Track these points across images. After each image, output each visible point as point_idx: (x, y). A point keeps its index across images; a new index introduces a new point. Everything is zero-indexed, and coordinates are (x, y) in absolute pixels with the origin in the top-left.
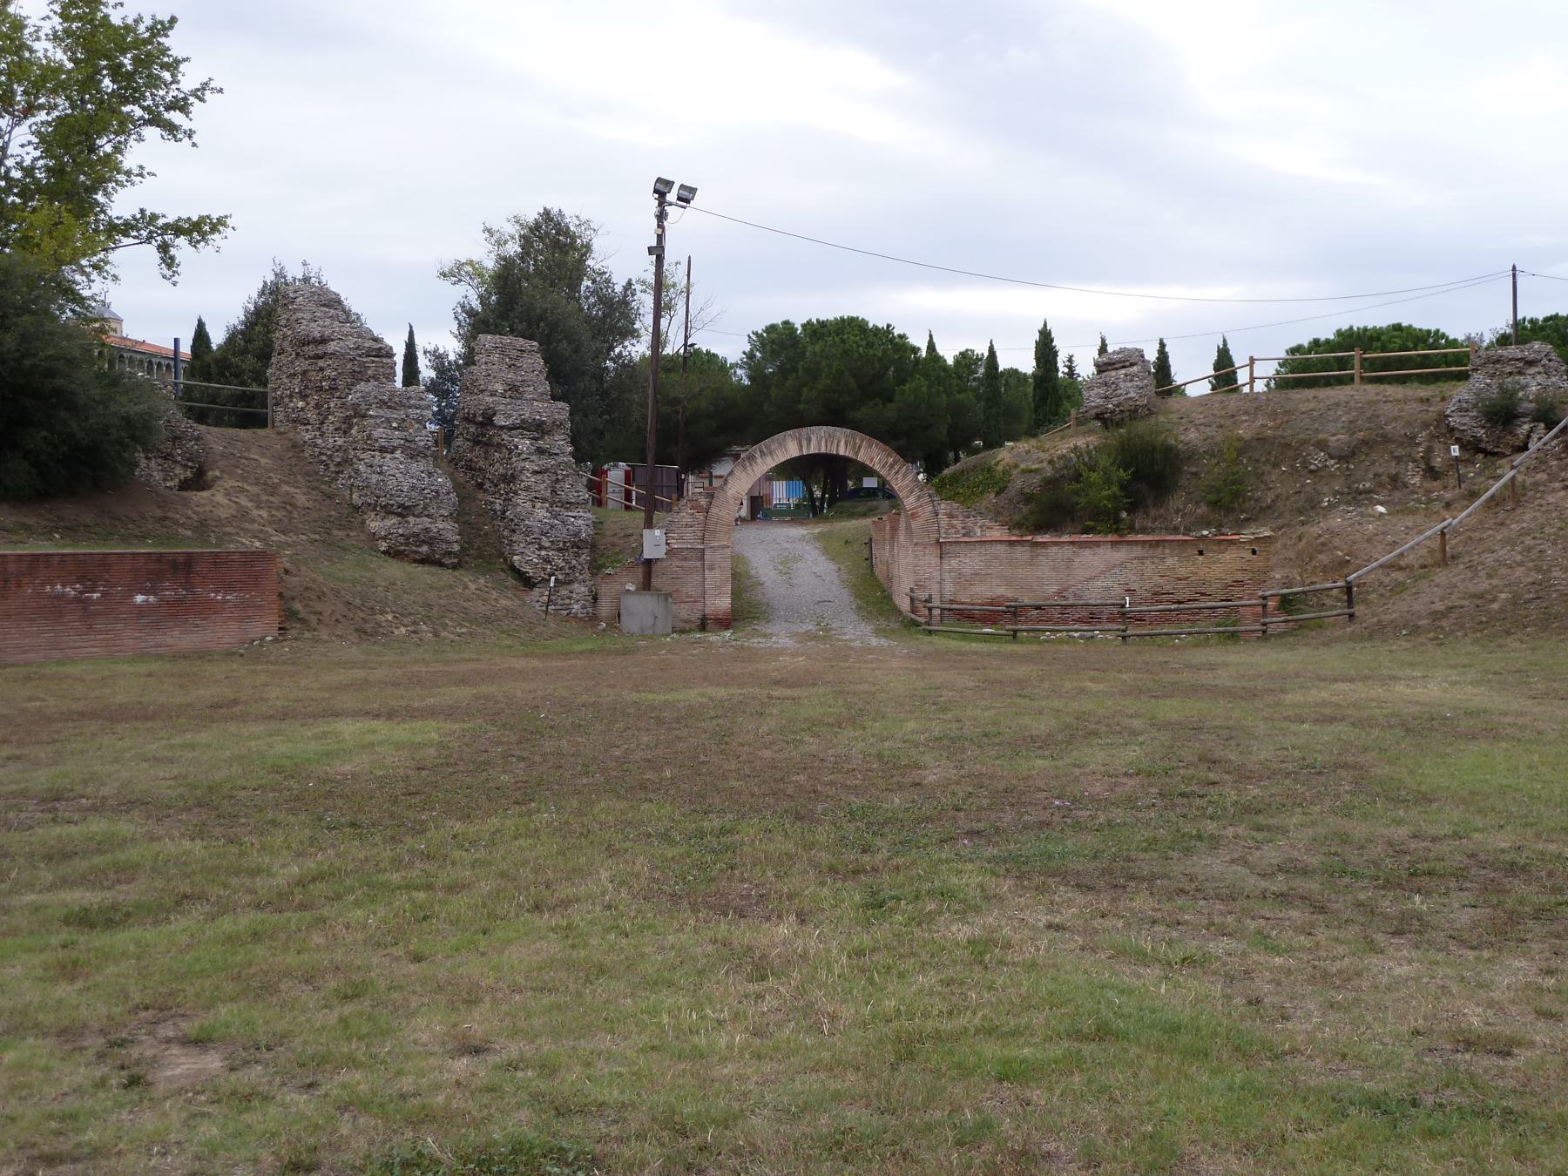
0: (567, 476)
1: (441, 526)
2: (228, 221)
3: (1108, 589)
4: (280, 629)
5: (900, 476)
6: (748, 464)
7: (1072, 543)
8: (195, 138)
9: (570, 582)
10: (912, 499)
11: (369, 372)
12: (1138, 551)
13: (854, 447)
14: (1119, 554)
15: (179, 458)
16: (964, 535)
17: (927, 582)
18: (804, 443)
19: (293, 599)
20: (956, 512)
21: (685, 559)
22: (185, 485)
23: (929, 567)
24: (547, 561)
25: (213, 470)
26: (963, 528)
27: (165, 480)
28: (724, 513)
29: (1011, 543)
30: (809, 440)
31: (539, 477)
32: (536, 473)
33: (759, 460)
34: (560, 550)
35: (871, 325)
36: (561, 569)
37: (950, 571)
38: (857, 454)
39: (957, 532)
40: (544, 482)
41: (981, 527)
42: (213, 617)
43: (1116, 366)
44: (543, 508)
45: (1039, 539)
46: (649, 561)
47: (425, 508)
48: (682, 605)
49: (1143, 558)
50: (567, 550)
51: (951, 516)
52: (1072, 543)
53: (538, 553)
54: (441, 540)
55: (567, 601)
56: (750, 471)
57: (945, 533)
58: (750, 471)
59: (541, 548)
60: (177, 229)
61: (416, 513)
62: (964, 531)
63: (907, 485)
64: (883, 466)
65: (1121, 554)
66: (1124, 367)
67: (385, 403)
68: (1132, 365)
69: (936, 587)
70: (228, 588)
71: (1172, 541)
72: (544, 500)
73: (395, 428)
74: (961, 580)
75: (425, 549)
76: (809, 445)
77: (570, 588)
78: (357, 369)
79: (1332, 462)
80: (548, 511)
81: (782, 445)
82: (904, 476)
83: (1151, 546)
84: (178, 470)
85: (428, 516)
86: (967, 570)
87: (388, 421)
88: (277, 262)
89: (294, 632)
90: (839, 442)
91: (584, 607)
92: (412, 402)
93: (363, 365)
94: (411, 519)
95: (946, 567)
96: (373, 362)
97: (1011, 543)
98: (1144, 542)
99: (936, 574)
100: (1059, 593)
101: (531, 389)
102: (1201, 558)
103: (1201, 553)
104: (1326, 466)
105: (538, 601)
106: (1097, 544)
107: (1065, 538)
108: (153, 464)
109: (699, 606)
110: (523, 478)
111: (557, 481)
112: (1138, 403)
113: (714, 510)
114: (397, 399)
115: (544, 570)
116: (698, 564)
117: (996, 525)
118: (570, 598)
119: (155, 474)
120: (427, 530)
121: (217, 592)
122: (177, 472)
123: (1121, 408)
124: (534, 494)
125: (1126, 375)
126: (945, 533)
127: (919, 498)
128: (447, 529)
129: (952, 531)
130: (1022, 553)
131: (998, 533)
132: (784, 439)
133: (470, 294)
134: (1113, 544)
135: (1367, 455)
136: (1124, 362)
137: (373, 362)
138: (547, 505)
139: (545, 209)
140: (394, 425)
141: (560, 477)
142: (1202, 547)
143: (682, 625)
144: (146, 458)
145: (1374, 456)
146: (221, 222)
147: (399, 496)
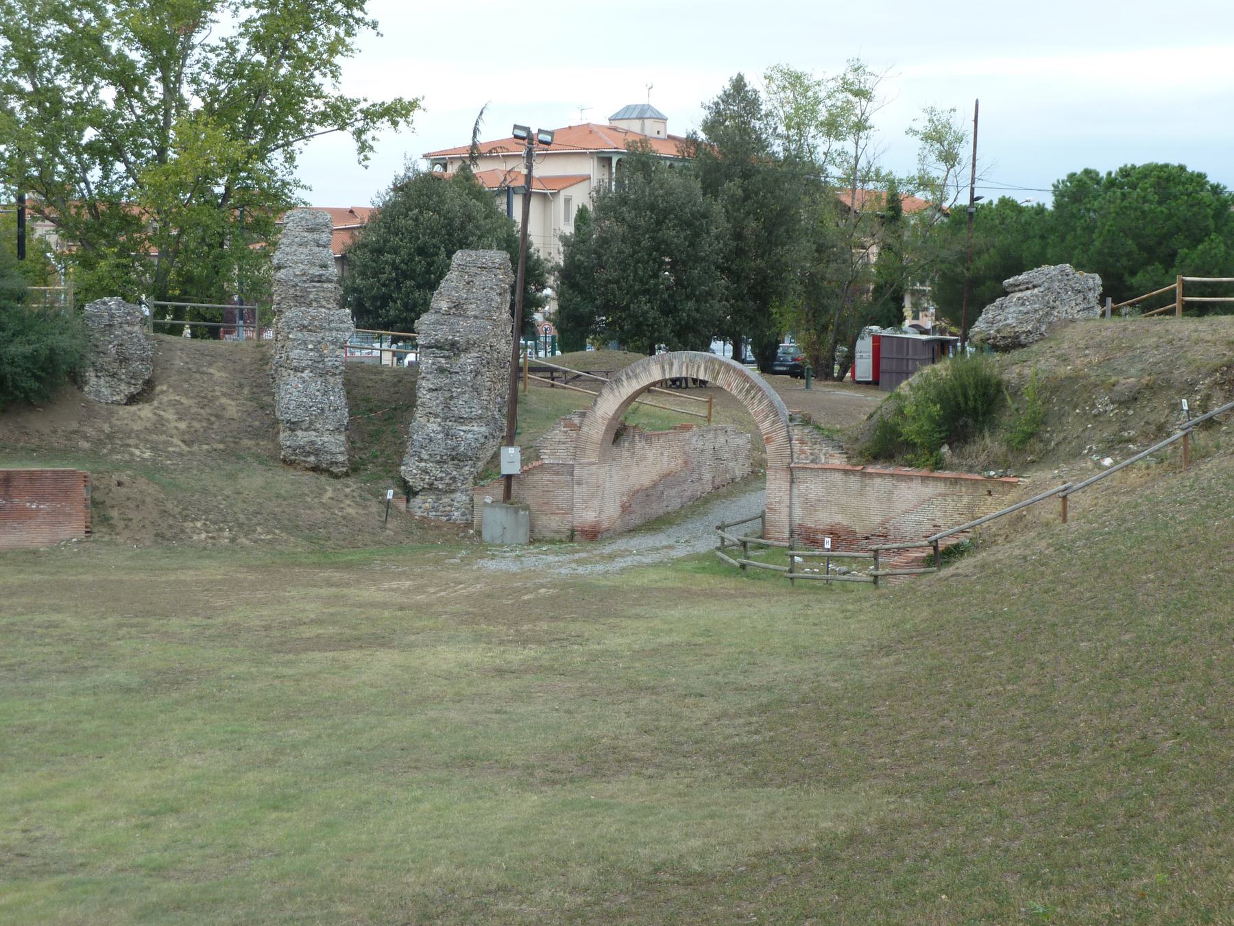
0: (464, 393)
1: (326, 440)
2: (421, 104)
3: (919, 523)
4: (87, 532)
5: (756, 401)
6: (615, 386)
7: (892, 475)
8: (379, 29)
9: (452, 491)
10: (767, 424)
11: (311, 296)
12: (941, 488)
13: (713, 372)
14: (927, 490)
15: (123, 377)
16: (812, 461)
17: (778, 506)
18: (667, 367)
19: (113, 507)
20: (806, 439)
21: (557, 474)
22: (132, 400)
23: (780, 491)
24: (426, 472)
25: (162, 384)
26: (812, 454)
27: (112, 395)
28: (593, 432)
29: (846, 472)
30: (671, 365)
31: (435, 394)
32: (431, 390)
33: (625, 383)
34: (438, 462)
35: (1049, 202)
36: (441, 479)
37: (799, 496)
38: (715, 379)
39: (806, 458)
40: (437, 399)
41: (825, 454)
42: (29, 521)
43: (1021, 287)
44: (434, 422)
45: (870, 470)
46: (509, 478)
47: (311, 423)
48: (553, 517)
49: (946, 495)
50: (445, 462)
51: (802, 442)
52: (892, 475)
53: (417, 463)
54: (326, 452)
55: (448, 508)
56: (617, 393)
57: (798, 458)
58: (617, 393)
59: (421, 460)
60: (372, 115)
61: (303, 427)
62: (812, 457)
63: (763, 411)
64: (741, 391)
65: (929, 490)
66: (1028, 289)
67: (305, 327)
68: (1034, 287)
69: (785, 511)
70: (41, 498)
71: (967, 479)
72: (437, 416)
73: (311, 350)
74: (812, 506)
75: (312, 459)
76: (671, 369)
77: (452, 496)
78: (299, 294)
79: (1112, 407)
80: (440, 425)
81: (646, 369)
82: (760, 402)
83: (951, 483)
84: (123, 387)
85: (315, 430)
86: (812, 496)
87: (305, 343)
88: (408, 157)
89: (97, 536)
90: (699, 367)
91: (463, 514)
92: (333, 325)
93: (304, 290)
94: (299, 433)
95: (795, 491)
96: (314, 287)
97: (846, 472)
98: (946, 479)
99: (786, 498)
100: (882, 524)
101: (474, 306)
102: (990, 499)
103: (990, 493)
104: (1106, 411)
105: (420, 508)
106: (909, 478)
107: (891, 470)
108: (102, 381)
109: (569, 518)
110: (420, 395)
111: (452, 398)
112: (1017, 329)
113: (585, 429)
114: (316, 323)
115: (424, 480)
116: (569, 478)
117: (836, 452)
118: (451, 506)
119: (103, 390)
120: (312, 443)
121: (32, 502)
122: (122, 388)
123: (1002, 334)
124: (428, 410)
125: (1019, 299)
126: (798, 458)
127: (774, 422)
128: (335, 444)
129: (803, 456)
130: (854, 482)
131: (838, 461)
132: (648, 364)
133: (868, 124)
134: (924, 479)
135: (1149, 400)
136: (1027, 283)
137: (314, 287)
138: (439, 420)
139: (739, 75)
140: (310, 346)
141: (455, 394)
142: (990, 487)
143: (552, 534)
144: (97, 376)
145: (1155, 402)
146: (413, 105)
147: (287, 413)
